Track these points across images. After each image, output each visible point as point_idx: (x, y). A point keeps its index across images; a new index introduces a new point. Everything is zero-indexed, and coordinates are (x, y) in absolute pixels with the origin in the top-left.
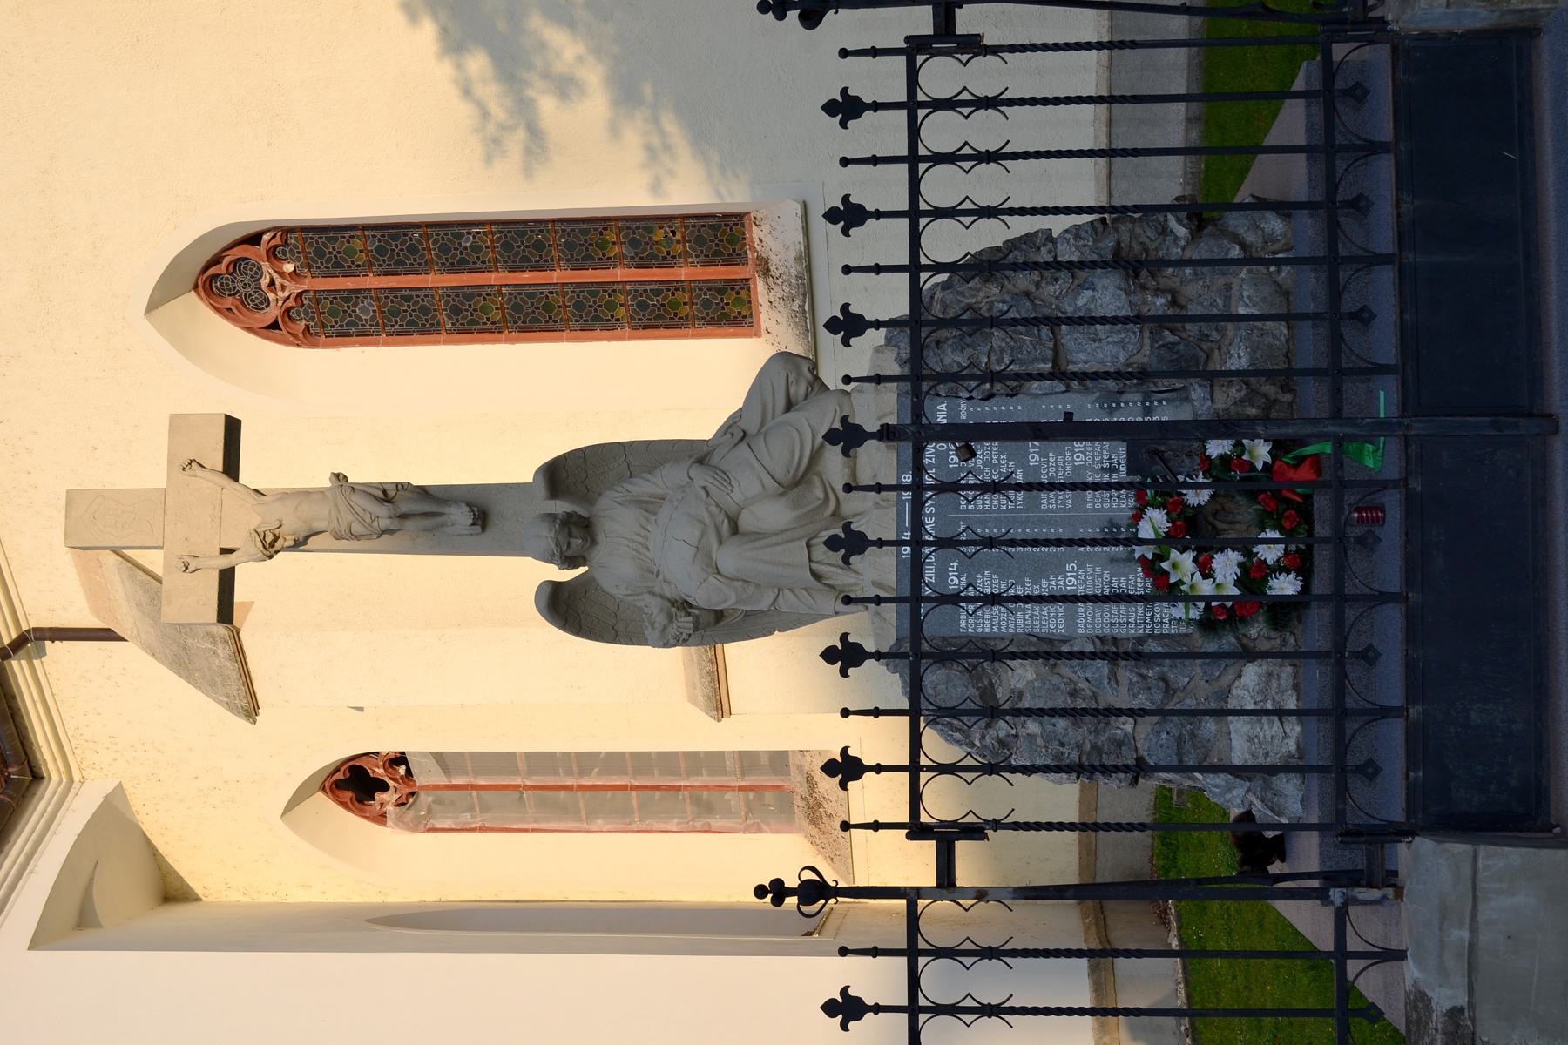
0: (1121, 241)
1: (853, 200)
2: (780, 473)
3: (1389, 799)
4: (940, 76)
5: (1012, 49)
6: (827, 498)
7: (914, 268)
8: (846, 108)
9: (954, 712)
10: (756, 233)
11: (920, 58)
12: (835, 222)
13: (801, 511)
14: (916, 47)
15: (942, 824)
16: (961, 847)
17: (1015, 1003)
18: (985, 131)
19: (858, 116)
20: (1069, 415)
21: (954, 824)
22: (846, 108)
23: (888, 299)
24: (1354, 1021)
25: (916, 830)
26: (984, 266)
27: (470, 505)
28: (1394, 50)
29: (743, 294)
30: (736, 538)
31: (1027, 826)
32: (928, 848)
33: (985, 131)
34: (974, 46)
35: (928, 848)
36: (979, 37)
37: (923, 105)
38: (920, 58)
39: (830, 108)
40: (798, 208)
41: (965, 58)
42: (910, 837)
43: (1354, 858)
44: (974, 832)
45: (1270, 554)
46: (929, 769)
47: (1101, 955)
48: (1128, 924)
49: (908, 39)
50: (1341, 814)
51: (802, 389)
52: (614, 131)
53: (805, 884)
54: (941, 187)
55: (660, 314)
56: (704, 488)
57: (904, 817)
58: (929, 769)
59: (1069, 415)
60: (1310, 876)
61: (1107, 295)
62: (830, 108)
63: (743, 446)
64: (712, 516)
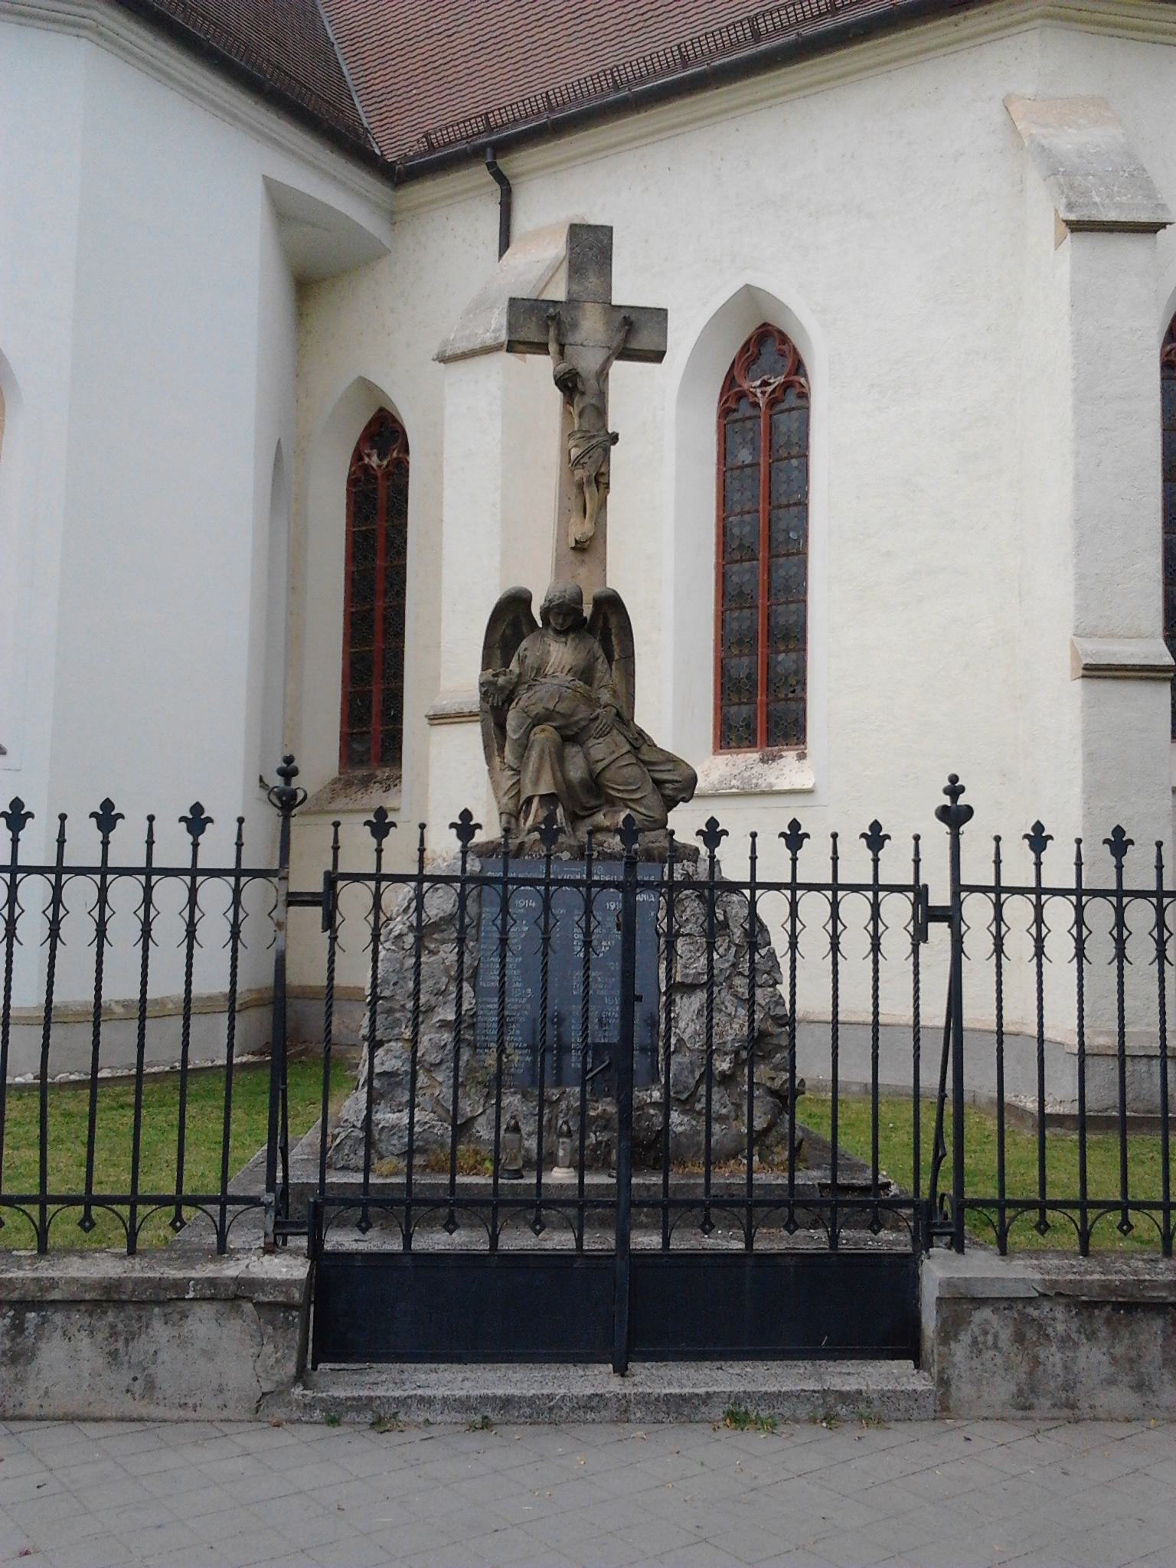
0: (772, 1037)
1: (806, 840)
2: (608, 775)
3: (340, 1240)
4: (898, 910)
5: (916, 965)
6: (587, 809)
7: (754, 885)
8: (875, 838)
9: (420, 908)
10: (790, 755)
11: (911, 895)
12: (707, 825)
13: (578, 788)
14: (920, 892)
15: (915, 916)
16: (317, 912)
17: (196, 950)
18: (856, 941)
19: (869, 846)
20: (639, 998)
21: (335, 907)
22: (875, 838)
23: (733, 866)
24: (172, 1209)
25: (332, 879)
26: (756, 932)
27: (591, 539)
28: (906, 1256)
29: (747, 743)
30: (559, 740)
31: (331, 961)
32: (318, 886)
33: (856, 941)
34: (920, 936)
35: (318, 886)
36: (925, 940)
37: (876, 896)
38: (911, 895)
39: (876, 826)
40: (809, 785)
41: (911, 928)
42: (327, 874)
43: (298, 1210)
44: (329, 923)
45: (796, 473)
46: (378, 888)
47: (232, 1003)
48: (253, 1025)
49: (926, 886)
50: (331, 1202)
51: (668, 792)
52: (1058, 244)
53: (294, 795)
54: (813, 906)
55: (730, 687)
56: (597, 718)
57: (342, 869)
58: (378, 888)
59: (639, 998)
60: (285, 1177)
61: (733, 1028)
62: (876, 826)
63: (628, 747)
64: (577, 722)
